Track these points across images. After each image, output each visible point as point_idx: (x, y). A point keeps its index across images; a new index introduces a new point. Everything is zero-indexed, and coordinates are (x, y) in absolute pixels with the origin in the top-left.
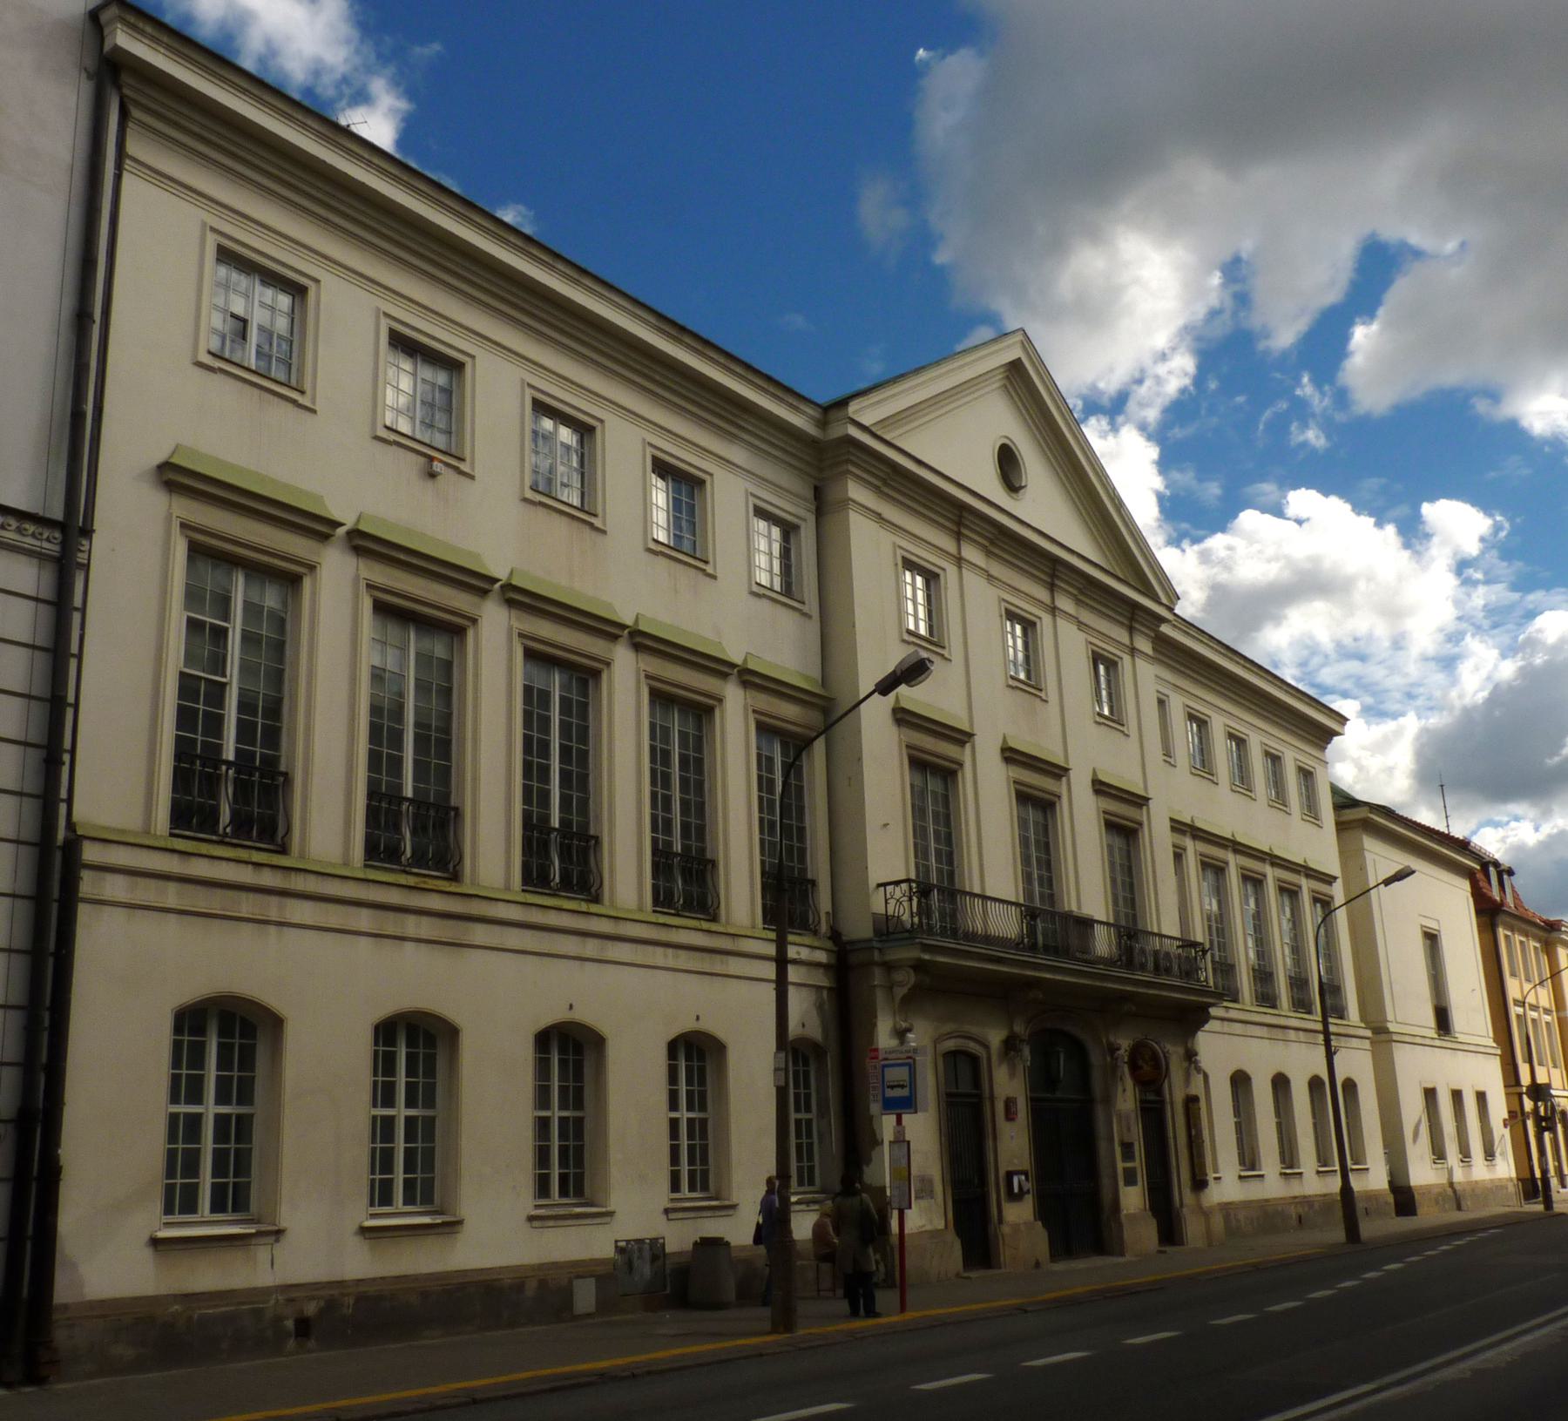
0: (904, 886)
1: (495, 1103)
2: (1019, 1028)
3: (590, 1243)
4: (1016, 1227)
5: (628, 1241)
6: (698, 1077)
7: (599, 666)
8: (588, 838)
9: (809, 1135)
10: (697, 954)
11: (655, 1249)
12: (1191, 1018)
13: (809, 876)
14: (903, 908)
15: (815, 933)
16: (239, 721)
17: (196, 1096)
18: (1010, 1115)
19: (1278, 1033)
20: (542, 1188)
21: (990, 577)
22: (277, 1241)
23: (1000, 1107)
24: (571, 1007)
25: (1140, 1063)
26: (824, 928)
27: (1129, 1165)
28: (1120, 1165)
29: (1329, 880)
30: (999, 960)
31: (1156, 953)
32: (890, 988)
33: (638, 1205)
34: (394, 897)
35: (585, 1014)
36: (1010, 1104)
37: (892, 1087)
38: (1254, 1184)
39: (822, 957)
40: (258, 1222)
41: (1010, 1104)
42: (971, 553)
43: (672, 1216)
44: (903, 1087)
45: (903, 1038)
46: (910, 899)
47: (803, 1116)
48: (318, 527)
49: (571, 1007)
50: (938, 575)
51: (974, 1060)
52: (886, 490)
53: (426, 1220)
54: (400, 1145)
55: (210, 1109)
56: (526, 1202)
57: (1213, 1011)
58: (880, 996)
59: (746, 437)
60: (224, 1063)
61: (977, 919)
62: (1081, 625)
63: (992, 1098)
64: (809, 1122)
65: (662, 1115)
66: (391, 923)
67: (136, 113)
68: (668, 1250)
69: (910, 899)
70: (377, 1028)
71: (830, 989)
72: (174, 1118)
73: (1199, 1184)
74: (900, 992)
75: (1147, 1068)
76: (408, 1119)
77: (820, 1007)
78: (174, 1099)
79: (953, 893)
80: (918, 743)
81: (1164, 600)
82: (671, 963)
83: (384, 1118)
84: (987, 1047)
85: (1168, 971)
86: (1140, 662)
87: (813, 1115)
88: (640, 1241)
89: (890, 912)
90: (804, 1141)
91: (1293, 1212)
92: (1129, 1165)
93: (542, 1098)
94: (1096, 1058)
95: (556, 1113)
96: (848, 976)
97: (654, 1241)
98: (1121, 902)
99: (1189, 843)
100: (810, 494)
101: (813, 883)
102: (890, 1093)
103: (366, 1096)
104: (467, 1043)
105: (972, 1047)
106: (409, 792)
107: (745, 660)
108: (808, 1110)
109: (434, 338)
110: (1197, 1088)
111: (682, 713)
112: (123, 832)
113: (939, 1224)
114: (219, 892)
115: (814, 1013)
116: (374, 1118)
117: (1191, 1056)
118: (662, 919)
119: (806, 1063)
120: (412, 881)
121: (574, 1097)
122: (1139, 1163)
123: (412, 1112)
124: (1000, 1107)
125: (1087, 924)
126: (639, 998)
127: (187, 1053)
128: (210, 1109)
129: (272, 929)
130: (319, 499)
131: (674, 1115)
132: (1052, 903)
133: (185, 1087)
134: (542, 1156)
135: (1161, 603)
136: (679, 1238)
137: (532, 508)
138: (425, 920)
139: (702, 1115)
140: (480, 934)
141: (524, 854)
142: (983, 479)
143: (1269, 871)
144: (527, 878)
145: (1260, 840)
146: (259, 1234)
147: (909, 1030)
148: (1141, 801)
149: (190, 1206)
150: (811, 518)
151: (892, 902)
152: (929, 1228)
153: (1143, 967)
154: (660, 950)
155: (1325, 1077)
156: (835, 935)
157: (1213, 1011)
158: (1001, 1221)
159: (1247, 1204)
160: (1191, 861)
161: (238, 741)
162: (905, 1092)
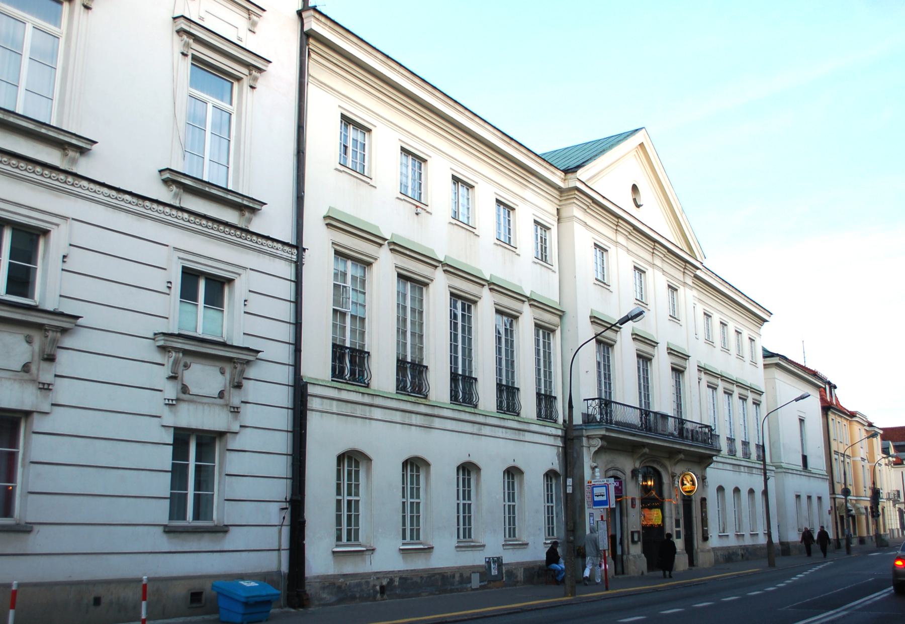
2: (637, 465)
3: (476, 559)
4: (634, 556)
6: (511, 486)
7: (372, 260)
8: (551, 397)
11: (498, 561)
12: (703, 461)
13: (425, 364)
14: (594, 409)
18: (633, 506)
19: (737, 468)
29: (760, 393)
30: (634, 435)
33: (492, 544)
34: (408, 407)
38: (725, 539)
39: (560, 433)
41: (633, 500)
45: (593, 471)
52: (588, 211)
56: (454, 542)
57: (714, 458)
58: (585, 450)
59: (531, 186)
61: (619, 414)
65: (399, 500)
66: (408, 418)
67: (313, 55)
73: (705, 538)
74: (593, 450)
77: (558, 456)
81: (699, 259)
82: (504, 436)
85: (697, 440)
86: (688, 290)
91: (740, 552)
96: (570, 440)
97: (498, 558)
99: (703, 375)
100: (555, 212)
101: (555, 398)
102: (596, 499)
108: (552, 502)
111: (463, 303)
112: (317, 379)
114: (350, 405)
118: (541, 423)
120: (413, 399)
122: (681, 529)
125: (665, 417)
126: (493, 451)
129: (368, 421)
130: (480, 271)
131: (339, 498)
140: (437, 423)
142: (622, 200)
143: (735, 388)
144: (334, 375)
145: (734, 375)
147: (596, 467)
150: (556, 224)
151: (591, 408)
153: (687, 438)
158: (629, 553)
159: (722, 549)
160: (704, 384)
162: (604, 498)
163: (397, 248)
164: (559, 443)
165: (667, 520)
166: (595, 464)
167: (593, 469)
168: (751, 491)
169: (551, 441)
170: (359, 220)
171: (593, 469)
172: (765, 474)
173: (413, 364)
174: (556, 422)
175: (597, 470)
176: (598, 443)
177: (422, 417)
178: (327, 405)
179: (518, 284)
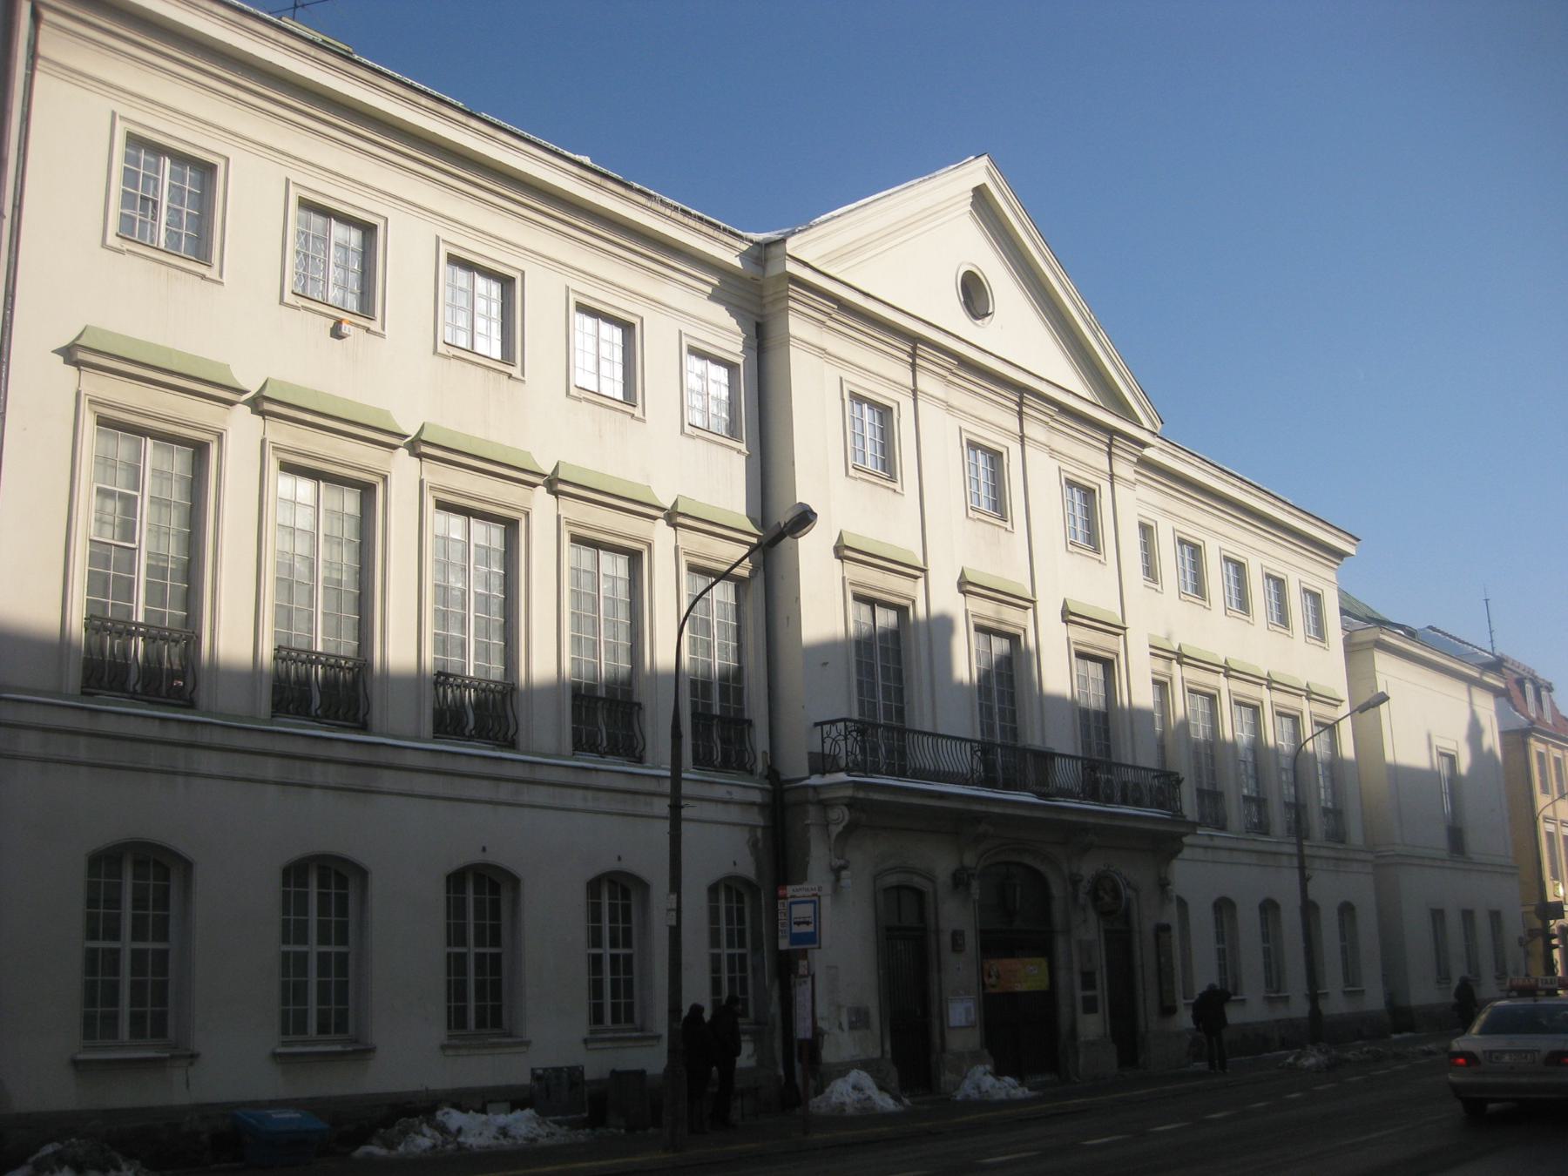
0: (841, 725)
1: (405, 945)
2: (969, 859)
5: (545, 1070)
9: (743, 969)
10: (620, 796)
12: (1163, 845)
15: (751, 772)
16: (148, 582)
17: (302, 938)
20: (597, 1016)
21: (949, 407)
22: (191, 1064)
23: (946, 939)
24: (484, 849)
25: (1101, 893)
26: (760, 767)
27: (1089, 993)
28: (1079, 994)
29: (1335, 702)
31: (1125, 785)
32: (826, 825)
35: (500, 856)
36: (957, 937)
37: (798, 924)
39: (756, 796)
40: (356, 1042)
41: (957, 937)
42: (1033, 430)
43: (590, 1046)
44: (808, 923)
46: (846, 739)
47: (737, 951)
48: (223, 392)
49: (484, 849)
50: (891, 409)
51: (920, 894)
53: (338, 1048)
54: (313, 978)
55: (313, 948)
57: (1186, 840)
58: (815, 835)
60: (323, 910)
62: (1052, 452)
63: (937, 931)
64: (743, 957)
68: (586, 1078)
69: (846, 739)
70: (448, 878)
71: (764, 828)
72: (285, 955)
74: (836, 830)
75: (1107, 899)
76: (612, 956)
77: (754, 845)
78: (285, 941)
79: (900, 731)
80: (862, 580)
81: (1147, 424)
83: (457, 954)
84: (931, 878)
87: (747, 950)
88: (558, 1070)
89: (827, 751)
90: (738, 974)
92: (1089, 993)
93: (456, 934)
94: (1057, 889)
95: (607, 951)
98: (1093, 732)
101: (750, 723)
102: (796, 929)
103: (276, 931)
104: (375, 884)
105: (917, 881)
106: (716, 710)
107: (676, 503)
109: (170, 136)
110: (1171, 915)
113: (877, 1054)
115: (747, 851)
116: (285, 955)
117: (1163, 885)
119: (740, 899)
121: (492, 934)
122: (1101, 992)
123: (615, 951)
124: (946, 939)
127: (293, 903)
128: (313, 948)
130: (386, 414)
131: (716, 951)
132: (1109, 754)
133: (293, 931)
134: (596, 989)
135: (1140, 425)
136: (597, 1064)
137: (446, 361)
138: (332, 768)
139: (627, 951)
141: (574, 721)
146: (354, 1052)
147: (844, 868)
148: (1117, 630)
149: (301, 1027)
151: (828, 742)
152: (863, 1057)
154: (579, 793)
155: (657, 874)
156: (773, 774)
157: (1186, 840)
158: (943, 1049)
161: (147, 602)
162: (810, 929)
163: (416, 447)
164: (756, 818)
165: (1062, 975)
166: (842, 862)
167: (837, 872)
168: (1269, 908)
169: (734, 814)
170: (169, 352)
171: (837, 872)
172: (1302, 868)
173: (724, 720)
174: (751, 772)
175: (844, 873)
176: (840, 815)
177: (720, 806)
178: (710, 811)
179: (639, 481)
